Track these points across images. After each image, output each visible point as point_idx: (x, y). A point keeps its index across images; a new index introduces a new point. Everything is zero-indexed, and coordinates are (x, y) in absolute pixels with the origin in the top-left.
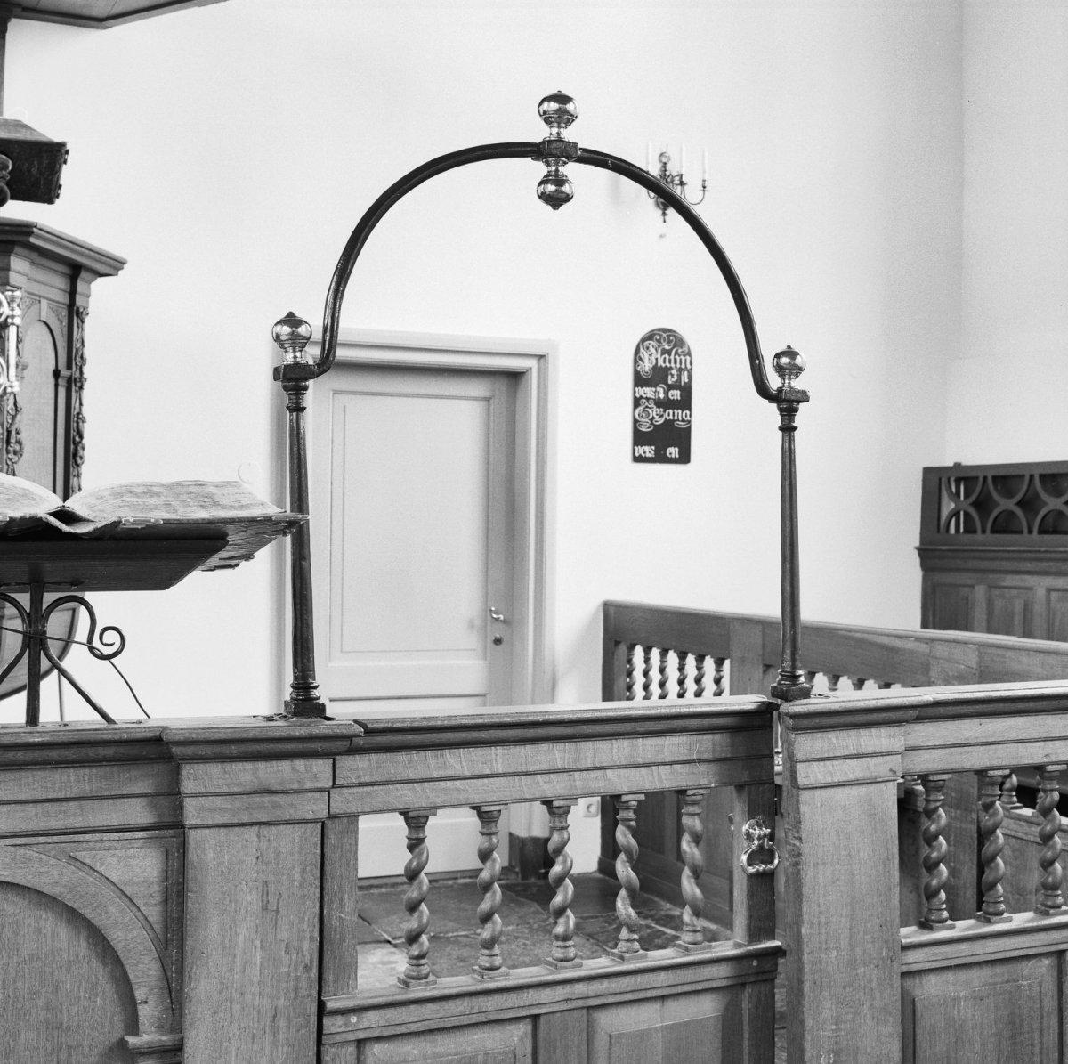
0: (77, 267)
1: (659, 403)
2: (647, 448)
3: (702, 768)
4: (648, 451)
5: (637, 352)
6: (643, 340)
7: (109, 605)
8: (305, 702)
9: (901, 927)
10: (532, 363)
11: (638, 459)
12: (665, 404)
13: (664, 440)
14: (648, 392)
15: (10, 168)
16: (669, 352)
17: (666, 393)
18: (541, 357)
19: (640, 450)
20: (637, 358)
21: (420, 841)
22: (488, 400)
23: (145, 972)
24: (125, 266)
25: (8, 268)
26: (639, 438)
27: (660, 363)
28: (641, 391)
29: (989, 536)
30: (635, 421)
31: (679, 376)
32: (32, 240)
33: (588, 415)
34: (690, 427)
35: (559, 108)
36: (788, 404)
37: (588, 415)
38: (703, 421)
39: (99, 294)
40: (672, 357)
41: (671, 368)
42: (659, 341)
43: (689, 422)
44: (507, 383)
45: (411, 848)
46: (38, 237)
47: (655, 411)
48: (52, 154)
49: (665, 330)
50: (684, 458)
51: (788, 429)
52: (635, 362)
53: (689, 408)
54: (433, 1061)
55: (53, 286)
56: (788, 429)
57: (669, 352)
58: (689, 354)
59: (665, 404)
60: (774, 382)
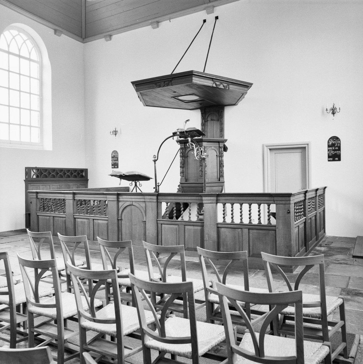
1: (333, 150)
4: (331, 159)
5: (328, 141)
6: (329, 139)
7: (141, 182)
10: (306, 146)
11: (329, 161)
12: (335, 150)
14: (331, 148)
15: (75, 358)
16: (335, 141)
17: (335, 148)
19: (329, 159)
20: (328, 142)
21: (225, 207)
22: (301, 152)
25: (192, 80)
26: (329, 157)
27: (333, 143)
28: (329, 148)
29: (65, 178)
30: (328, 154)
31: (338, 145)
32: (193, 73)
33: (319, 151)
34: (340, 154)
42: (333, 139)
43: (340, 153)
44: (303, 149)
45: (223, 208)
46: (194, 72)
47: (332, 152)
49: (331, 138)
50: (339, 160)
51: (155, 164)
52: (328, 143)
53: (340, 151)
56: (155, 164)
57: (335, 141)
58: (340, 140)
59: (335, 150)
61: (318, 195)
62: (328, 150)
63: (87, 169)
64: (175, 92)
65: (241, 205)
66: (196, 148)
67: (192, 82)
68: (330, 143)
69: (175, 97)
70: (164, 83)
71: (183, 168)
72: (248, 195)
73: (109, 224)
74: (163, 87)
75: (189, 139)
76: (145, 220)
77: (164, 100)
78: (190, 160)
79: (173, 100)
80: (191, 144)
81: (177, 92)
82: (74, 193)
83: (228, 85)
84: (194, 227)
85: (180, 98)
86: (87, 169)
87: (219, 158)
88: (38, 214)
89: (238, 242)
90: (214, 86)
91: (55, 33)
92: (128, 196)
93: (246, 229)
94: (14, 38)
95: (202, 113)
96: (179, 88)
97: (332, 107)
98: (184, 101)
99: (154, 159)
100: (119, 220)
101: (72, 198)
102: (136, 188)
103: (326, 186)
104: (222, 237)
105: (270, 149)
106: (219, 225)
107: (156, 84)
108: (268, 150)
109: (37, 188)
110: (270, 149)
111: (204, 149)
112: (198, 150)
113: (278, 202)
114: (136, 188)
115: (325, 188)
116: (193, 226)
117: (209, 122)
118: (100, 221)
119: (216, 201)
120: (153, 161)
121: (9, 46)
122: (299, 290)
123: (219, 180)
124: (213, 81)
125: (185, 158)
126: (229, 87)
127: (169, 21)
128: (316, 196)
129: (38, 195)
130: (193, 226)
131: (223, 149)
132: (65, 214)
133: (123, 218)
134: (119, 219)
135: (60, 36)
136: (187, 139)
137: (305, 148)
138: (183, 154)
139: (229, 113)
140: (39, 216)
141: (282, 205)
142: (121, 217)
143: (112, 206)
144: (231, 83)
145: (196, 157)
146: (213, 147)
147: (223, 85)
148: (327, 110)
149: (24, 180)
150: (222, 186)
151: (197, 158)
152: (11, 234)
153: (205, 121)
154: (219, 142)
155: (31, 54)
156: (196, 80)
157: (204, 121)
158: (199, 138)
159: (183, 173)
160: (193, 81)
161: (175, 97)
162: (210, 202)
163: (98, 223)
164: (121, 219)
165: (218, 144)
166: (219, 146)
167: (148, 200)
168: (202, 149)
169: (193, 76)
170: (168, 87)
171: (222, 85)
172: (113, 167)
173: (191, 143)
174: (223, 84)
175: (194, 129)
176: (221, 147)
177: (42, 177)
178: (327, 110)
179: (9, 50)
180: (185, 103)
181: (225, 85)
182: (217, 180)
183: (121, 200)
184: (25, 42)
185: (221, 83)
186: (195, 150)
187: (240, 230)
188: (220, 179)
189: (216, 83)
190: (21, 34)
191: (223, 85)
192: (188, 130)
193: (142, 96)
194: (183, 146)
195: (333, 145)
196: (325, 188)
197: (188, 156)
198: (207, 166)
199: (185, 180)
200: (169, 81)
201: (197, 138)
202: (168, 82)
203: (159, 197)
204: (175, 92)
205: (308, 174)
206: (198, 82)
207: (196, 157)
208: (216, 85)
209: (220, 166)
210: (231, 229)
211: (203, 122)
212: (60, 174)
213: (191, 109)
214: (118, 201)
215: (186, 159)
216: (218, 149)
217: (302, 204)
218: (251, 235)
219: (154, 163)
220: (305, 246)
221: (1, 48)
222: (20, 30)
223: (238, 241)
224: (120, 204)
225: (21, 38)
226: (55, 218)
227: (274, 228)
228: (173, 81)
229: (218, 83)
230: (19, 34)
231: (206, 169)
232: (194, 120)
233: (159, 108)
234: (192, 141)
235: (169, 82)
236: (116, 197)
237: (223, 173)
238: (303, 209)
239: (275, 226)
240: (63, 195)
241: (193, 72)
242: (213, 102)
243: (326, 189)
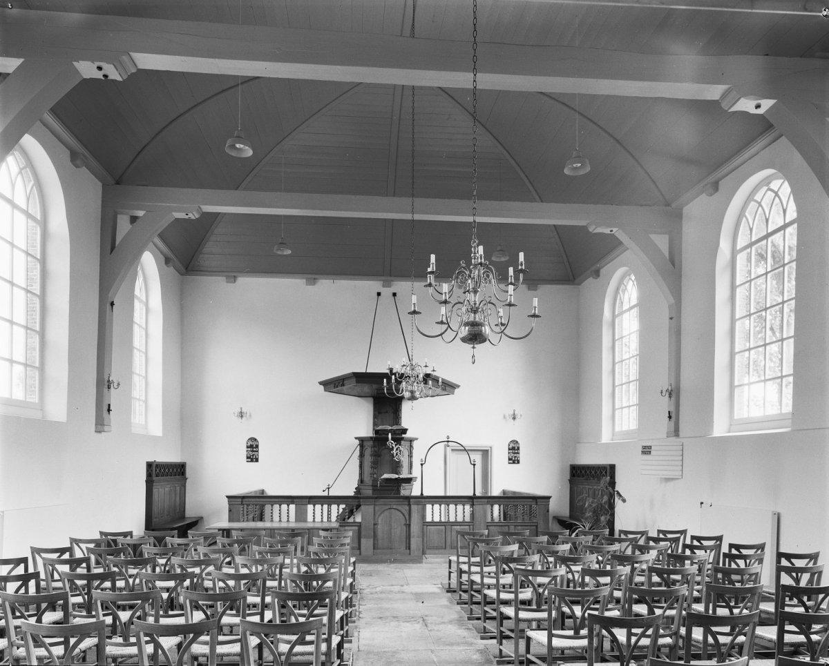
0: (411, 441)
4: (250, 460)
8: (422, 494)
9: (694, 603)
13: (514, 460)
20: (509, 445)
23: (407, 517)
24: (456, 391)
26: (510, 459)
33: (500, 456)
35: (448, 437)
36: (474, 465)
37: (500, 456)
38: (522, 455)
39: (415, 444)
47: (250, 453)
48: (407, 430)
55: (408, 443)
60: (472, 463)
65: (433, 505)
68: (511, 446)
110: (452, 450)
122: (818, 565)
137: (487, 451)
221: (2, 192)
239: (360, 523)
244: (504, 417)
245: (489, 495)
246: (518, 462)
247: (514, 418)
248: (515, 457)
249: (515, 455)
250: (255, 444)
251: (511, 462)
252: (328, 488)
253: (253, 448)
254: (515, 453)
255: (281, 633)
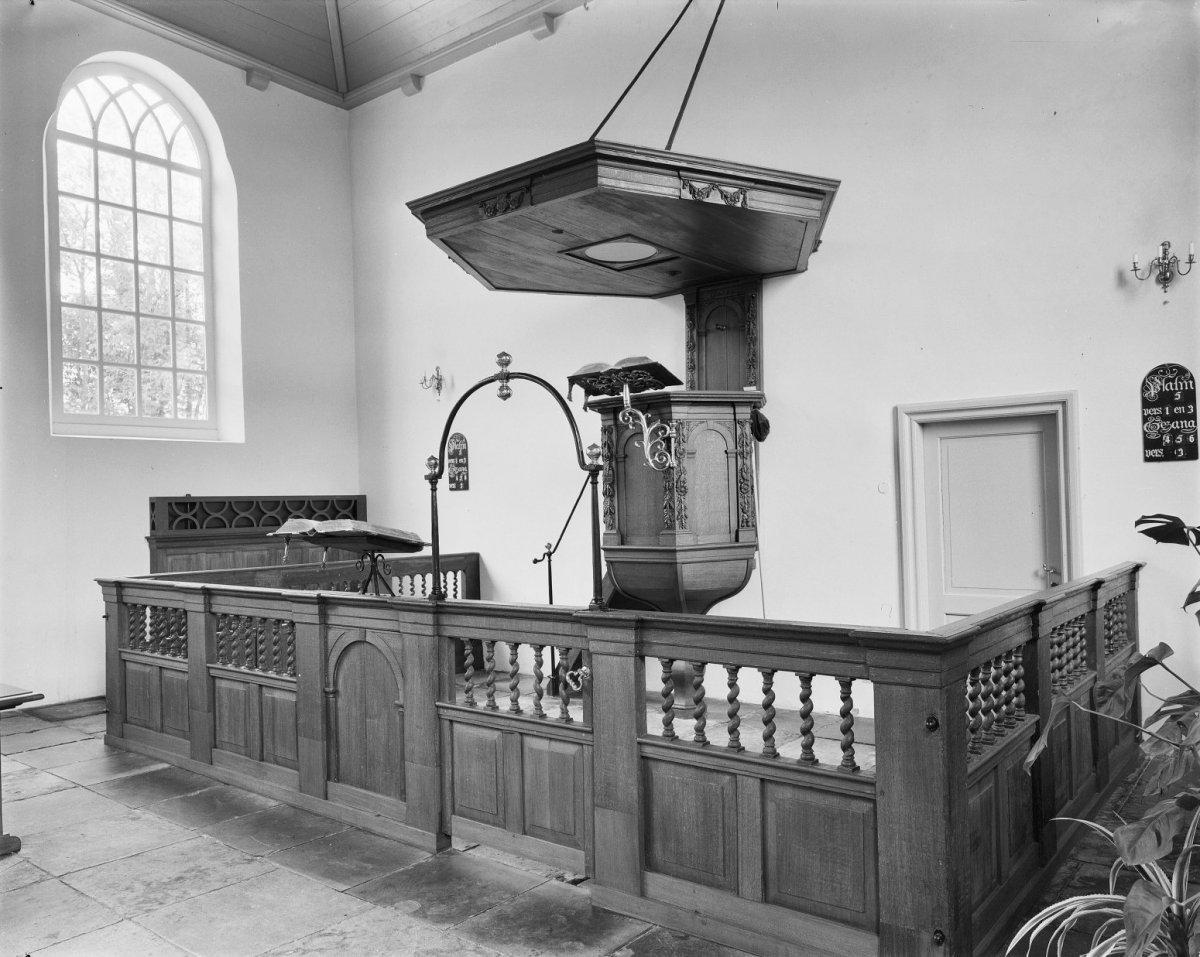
2: (1156, 451)
3: (445, 623)
5: (1144, 383)
11: (1148, 459)
14: (1156, 411)
16: (1173, 380)
18: (1064, 403)
19: (1150, 453)
20: (1145, 388)
25: (671, 413)
26: (1149, 444)
27: (1165, 388)
28: (1148, 412)
30: (1145, 433)
32: (442, 575)
35: (504, 359)
40: (1176, 383)
41: (1175, 391)
44: (1047, 425)
49: (1154, 372)
51: (434, 490)
52: (1143, 391)
54: (317, 954)
56: (434, 490)
57: (1173, 380)
58: (1192, 378)
60: (588, 461)
61: (1101, 604)
62: (1145, 419)
63: (365, 496)
64: (560, 231)
66: (649, 425)
67: (595, 184)
69: (573, 252)
70: (508, 196)
71: (611, 496)
72: (757, 633)
73: (301, 705)
74: (505, 212)
75: (626, 395)
76: (401, 701)
77: (541, 264)
78: (633, 471)
79: (568, 263)
80: (630, 414)
81: (566, 229)
82: (208, 589)
83: (743, 191)
84: (553, 743)
85: (591, 252)
86: (365, 496)
87: (734, 460)
88: (125, 656)
89: (720, 830)
90: (687, 195)
91: (248, 82)
92: (351, 609)
93: (751, 780)
94: (113, 98)
95: (687, 307)
96: (563, 210)
97: (1161, 255)
98: (612, 266)
99: (428, 472)
100: (330, 695)
101: (201, 608)
102: (376, 579)
103: (1139, 562)
104: (661, 801)
105: (923, 425)
106: (649, 751)
107: (483, 204)
108: (916, 427)
109: (189, 560)
110: (923, 425)
111: (678, 430)
112: (654, 433)
113: (886, 675)
114: (376, 579)
115: (1137, 568)
116: (551, 739)
117: (711, 336)
118: (277, 695)
119: (633, 646)
120: (426, 477)
121: (169, 147)
123: (737, 540)
124: (680, 177)
125: (617, 463)
126: (745, 198)
127: (582, 7)
128: (1093, 611)
129: (124, 593)
130: (547, 742)
131: (748, 429)
132: (186, 660)
133: (341, 688)
134: (327, 689)
135: (261, 88)
136: (626, 393)
137: (1053, 416)
138: (609, 448)
139: (778, 305)
140: (127, 663)
141: (903, 690)
142: (335, 683)
143: (308, 639)
144: (753, 184)
145: (650, 461)
146: (711, 423)
147: (721, 192)
148: (1135, 269)
149: (147, 538)
150: (748, 559)
151: (654, 462)
152: (87, 708)
153: (698, 333)
154: (733, 405)
155: (138, 139)
156: (610, 178)
157: (695, 333)
158: (658, 391)
159: (612, 514)
160: (601, 180)
161: (573, 252)
162: (611, 648)
163: (273, 699)
164: (336, 693)
165: (731, 410)
166: (735, 419)
167: (410, 628)
168: (671, 432)
169: (599, 161)
170: (525, 211)
171: (717, 191)
172: (454, 485)
173: (629, 409)
174: (724, 188)
175: (642, 363)
176: (740, 423)
177: (204, 526)
178: (1135, 269)
179: (133, 148)
180: (619, 270)
181: (731, 190)
182: (724, 538)
183: (332, 620)
184: (150, 110)
185: (714, 186)
186: (647, 432)
187: (728, 777)
188: (741, 534)
189: (691, 186)
190: (138, 87)
191: (721, 192)
192: (620, 368)
193: (457, 248)
194: (611, 423)
195: (1165, 399)
196: (1137, 568)
197: (626, 456)
198: (689, 491)
199: (617, 539)
200: (520, 189)
201: (651, 391)
202: (519, 192)
203: (445, 620)
204: (560, 231)
205: (1068, 517)
206: (623, 185)
207: (650, 461)
208: (692, 191)
209: (739, 489)
210: (692, 771)
211: (692, 337)
212: (269, 514)
213: (652, 293)
214: (324, 624)
215: (621, 465)
216: (732, 427)
217: (1020, 659)
218: (771, 807)
219: (429, 486)
220: (1037, 839)
222: (134, 74)
223: (720, 825)
224: (332, 635)
225: (137, 98)
226: (165, 672)
227: (868, 790)
228: (534, 190)
229: (698, 185)
230: (130, 88)
231: (687, 500)
232: (656, 332)
233: (545, 295)
234: (637, 402)
235: (523, 194)
236: (317, 612)
237: (750, 514)
238: (1022, 681)
240: (180, 596)
241: (594, 147)
242: (723, 262)
243: (1141, 573)
244: (1121, 280)
245: (431, 561)
246: (466, 487)
247: (439, 388)
248: (1174, 433)
249: (460, 469)
250: (1177, 389)
251: (1157, 452)
252: (549, 555)
253: (459, 458)
254: (1174, 417)
255: (164, 770)
